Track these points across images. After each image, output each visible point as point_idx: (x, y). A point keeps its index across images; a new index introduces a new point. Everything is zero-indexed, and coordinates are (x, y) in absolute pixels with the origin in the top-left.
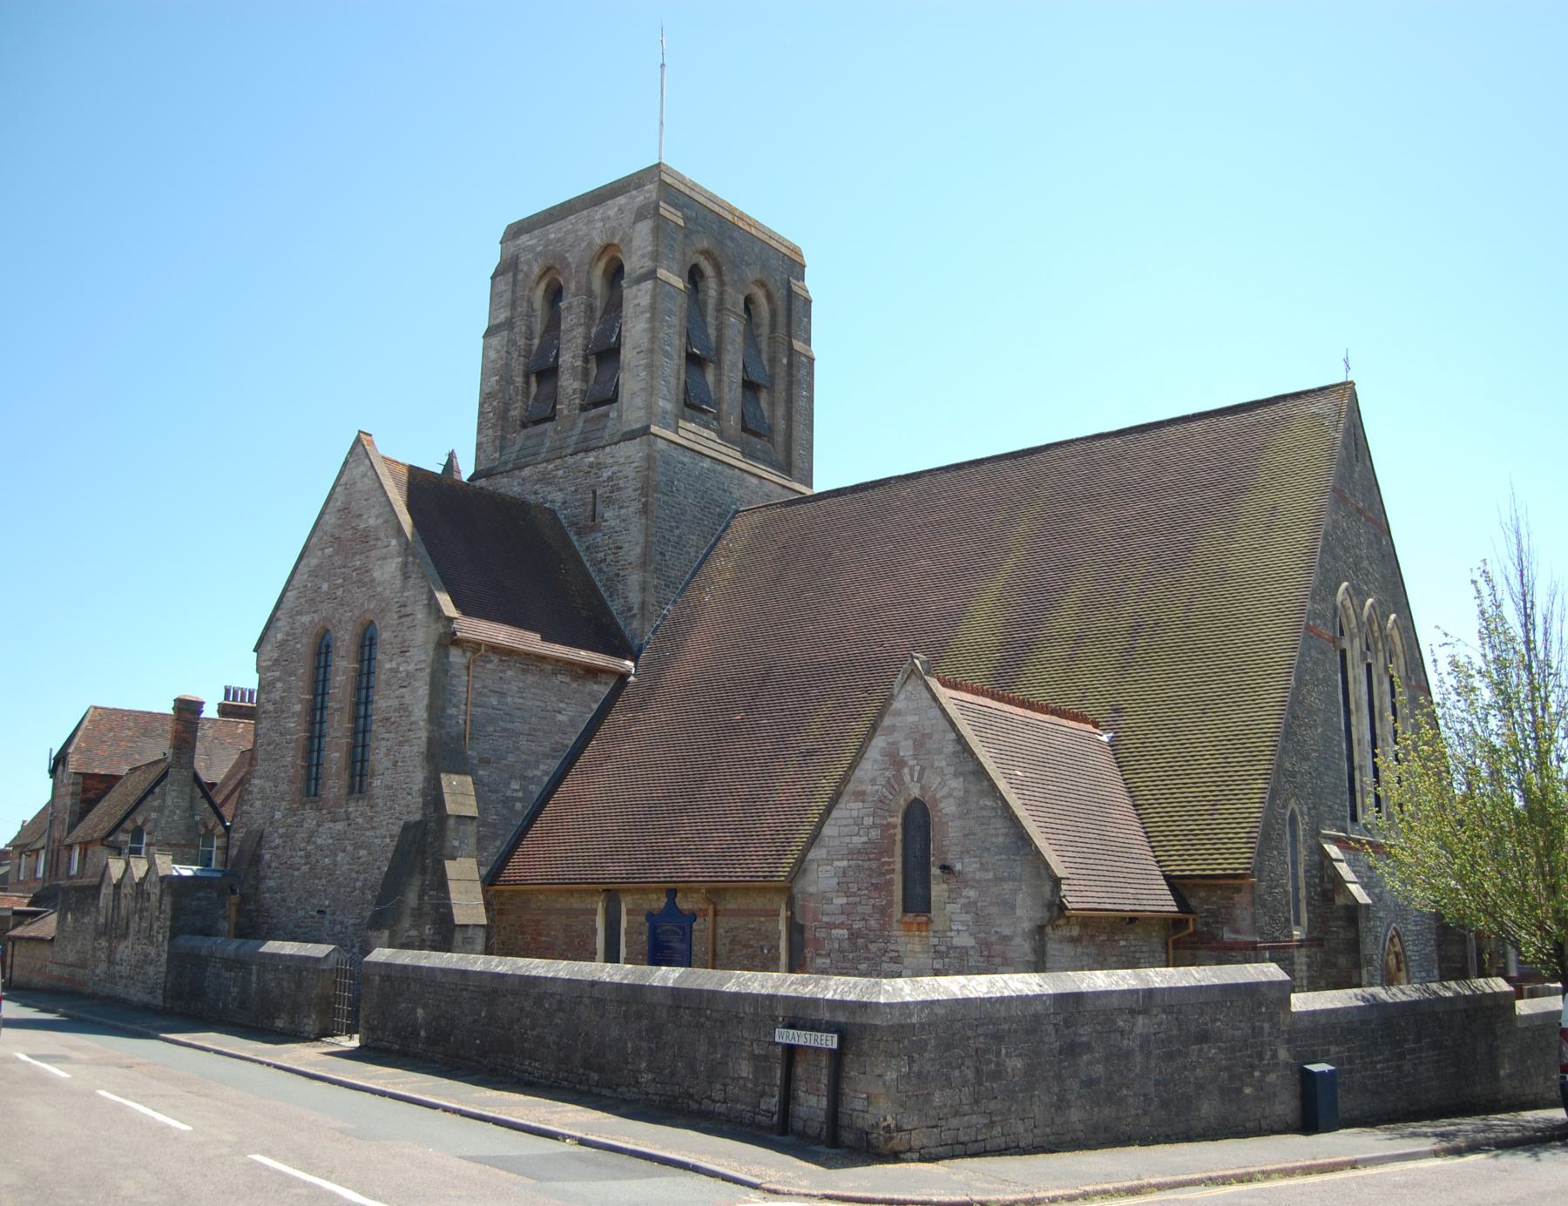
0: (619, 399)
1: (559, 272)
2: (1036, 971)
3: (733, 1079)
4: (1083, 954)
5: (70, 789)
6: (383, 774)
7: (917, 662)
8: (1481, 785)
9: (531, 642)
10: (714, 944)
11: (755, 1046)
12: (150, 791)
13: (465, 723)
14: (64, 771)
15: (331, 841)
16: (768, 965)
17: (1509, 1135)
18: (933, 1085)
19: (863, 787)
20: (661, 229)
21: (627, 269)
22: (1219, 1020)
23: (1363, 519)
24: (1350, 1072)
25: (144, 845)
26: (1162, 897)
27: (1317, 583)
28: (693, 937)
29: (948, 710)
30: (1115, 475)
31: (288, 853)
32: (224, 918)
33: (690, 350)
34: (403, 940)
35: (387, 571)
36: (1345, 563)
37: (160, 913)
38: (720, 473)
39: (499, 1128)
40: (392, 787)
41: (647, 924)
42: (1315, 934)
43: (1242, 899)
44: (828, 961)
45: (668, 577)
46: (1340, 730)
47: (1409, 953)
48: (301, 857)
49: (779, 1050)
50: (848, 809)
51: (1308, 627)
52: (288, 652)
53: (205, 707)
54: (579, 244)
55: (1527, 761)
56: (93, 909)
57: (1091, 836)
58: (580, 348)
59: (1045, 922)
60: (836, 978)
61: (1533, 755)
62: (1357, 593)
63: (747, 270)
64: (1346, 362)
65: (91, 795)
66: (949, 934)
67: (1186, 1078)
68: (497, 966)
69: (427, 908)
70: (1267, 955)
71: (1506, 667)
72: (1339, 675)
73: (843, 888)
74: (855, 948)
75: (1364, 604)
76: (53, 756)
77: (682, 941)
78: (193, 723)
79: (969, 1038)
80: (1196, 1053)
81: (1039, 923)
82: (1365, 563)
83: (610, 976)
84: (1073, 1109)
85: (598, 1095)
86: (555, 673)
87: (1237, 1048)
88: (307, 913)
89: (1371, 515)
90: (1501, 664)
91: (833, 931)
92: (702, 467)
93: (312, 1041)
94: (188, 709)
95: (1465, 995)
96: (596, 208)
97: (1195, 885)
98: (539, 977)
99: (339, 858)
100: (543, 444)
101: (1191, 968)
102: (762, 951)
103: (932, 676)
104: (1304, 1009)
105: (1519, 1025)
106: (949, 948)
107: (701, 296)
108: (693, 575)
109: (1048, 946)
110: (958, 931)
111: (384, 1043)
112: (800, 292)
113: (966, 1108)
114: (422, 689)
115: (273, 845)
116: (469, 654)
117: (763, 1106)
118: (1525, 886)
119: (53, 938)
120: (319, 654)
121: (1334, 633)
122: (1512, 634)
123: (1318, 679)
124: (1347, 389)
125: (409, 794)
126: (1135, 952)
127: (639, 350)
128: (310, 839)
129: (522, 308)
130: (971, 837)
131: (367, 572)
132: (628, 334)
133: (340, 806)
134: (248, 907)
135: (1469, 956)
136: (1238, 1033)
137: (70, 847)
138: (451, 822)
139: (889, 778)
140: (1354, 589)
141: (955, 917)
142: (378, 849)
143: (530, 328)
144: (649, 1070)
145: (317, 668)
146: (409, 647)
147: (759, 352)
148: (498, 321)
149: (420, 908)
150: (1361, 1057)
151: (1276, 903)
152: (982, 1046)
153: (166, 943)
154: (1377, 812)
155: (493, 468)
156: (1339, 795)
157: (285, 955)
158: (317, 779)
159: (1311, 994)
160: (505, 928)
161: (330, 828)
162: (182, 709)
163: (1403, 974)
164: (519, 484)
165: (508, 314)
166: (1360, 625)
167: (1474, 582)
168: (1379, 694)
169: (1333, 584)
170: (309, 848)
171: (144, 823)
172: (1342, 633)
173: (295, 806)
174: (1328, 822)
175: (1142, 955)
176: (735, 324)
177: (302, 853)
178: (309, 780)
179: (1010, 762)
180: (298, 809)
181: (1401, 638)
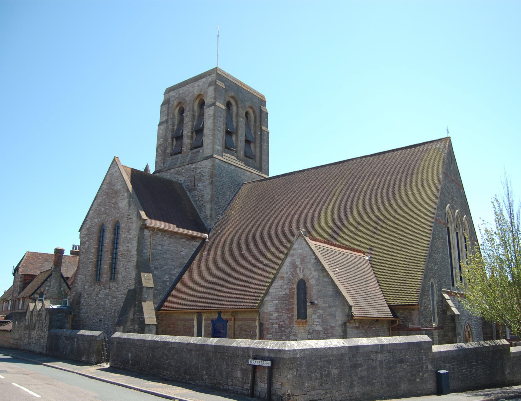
0: (203, 146)
1: (183, 104)
2: (343, 338)
3: (235, 377)
4: (360, 332)
5: (20, 279)
6: (121, 273)
7: (301, 231)
8: (497, 272)
9: (173, 228)
10: (234, 330)
11: (242, 366)
12: (46, 280)
13: (150, 255)
14: (18, 273)
15: (104, 296)
16: (253, 337)
17: (510, 395)
18: (305, 379)
19: (282, 275)
20: (217, 87)
21: (206, 102)
22: (407, 355)
23: (454, 183)
24: (454, 373)
25: (44, 298)
26: (387, 313)
27: (439, 204)
28: (227, 328)
29: (312, 248)
30: (370, 169)
31: (90, 300)
32: (67, 323)
33: (227, 130)
34: (128, 330)
35: (123, 203)
36: (449, 198)
37: (45, 321)
38: (238, 171)
39: (152, 395)
40: (124, 277)
41: (211, 324)
42: (440, 325)
43: (415, 313)
44: (272, 336)
45: (219, 206)
46: (448, 254)
47: (473, 331)
48: (94, 302)
49: (251, 367)
50: (278, 283)
51: (436, 219)
52: (90, 232)
53: (65, 252)
54: (190, 95)
55: (512, 264)
56: (24, 320)
57: (362, 291)
58: (190, 129)
59: (346, 321)
60: (271, 341)
61: (514, 262)
62: (453, 208)
63: (246, 103)
64: (447, 130)
65: (26, 281)
66: (313, 326)
67: (396, 376)
68: (155, 338)
69: (136, 319)
70: (424, 332)
71: (504, 231)
72: (447, 236)
73: (277, 310)
74: (281, 331)
75: (455, 212)
76: (14, 268)
77: (223, 330)
78: (61, 257)
79: (318, 362)
80: (399, 367)
81: (344, 322)
82: (455, 198)
83: (193, 341)
84: (356, 387)
85: (189, 383)
86: (181, 238)
87: (414, 365)
88: (96, 321)
89: (457, 182)
90: (503, 231)
91: (273, 325)
92: (231, 169)
93: (94, 365)
94: (59, 252)
95: (493, 346)
96: (195, 82)
97: (399, 308)
98: (169, 342)
99: (107, 302)
100: (177, 161)
101: (397, 337)
102: (251, 333)
103: (307, 236)
104: (437, 351)
105: (512, 356)
106: (313, 331)
107: (231, 112)
108: (228, 205)
109: (348, 330)
110: (316, 325)
111: (118, 366)
112: (264, 110)
113: (317, 387)
114: (135, 244)
115: (84, 297)
116: (151, 232)
117: (245, 387)
118: (513, 307)
119: (11, 330)
120: (101, 232)
121: (445, 221)
122: (506, 220)
123: (440, 237)
124: (448, 139)
125: (130, 280)
126: (378, 332)
127: (210, 129)
128: (97, 296)
129: (171, 116)
130: (321, 292)
131: (117, 204)
132: (206, 124)
133: (107, 284)
134: (76, 319)
135: (493, 332)
136: (414, 360)
137: (19, 299)
138: (145, 289)
139: (292, 272)
140: (452, 207)
141: (315, 320)
142: (120, 299)
143: (173, 122)
144: (206, 374)
145: (100, 237)
146: (130, 229)
147: (251, 130)
148: (163, 120)
149: (133, 319)
150: (457, 368)
151: (427, 314)
152: (323, 365)
153: (47, 331)
154: (461, 282)
155: (160, 170)
156: (448, 277)
157: (85, 335)
158: (99, 275)
159: (439, 346)
160: (163, 326)
161: (104, 292)
162: (57, 252)
163: (471, 339)
164: (169, 175)
165: (166, 118)
166: (454, 219)
167: (492, 202)
168: (461, 242)
169: (444, 205)
170: (96, 298)
171: (44, 291)
172: (448, 222)
173: (92, 284)
174: (444, 286)
175: (381, 333)
176: (242, 121)
177: (94, 300)
178: (97, 275)
179: (334, 266)
180: (93, 285)
181: (468, 224)
